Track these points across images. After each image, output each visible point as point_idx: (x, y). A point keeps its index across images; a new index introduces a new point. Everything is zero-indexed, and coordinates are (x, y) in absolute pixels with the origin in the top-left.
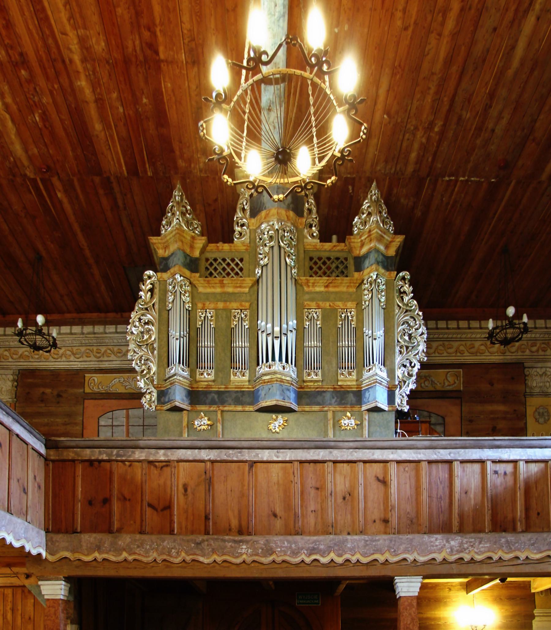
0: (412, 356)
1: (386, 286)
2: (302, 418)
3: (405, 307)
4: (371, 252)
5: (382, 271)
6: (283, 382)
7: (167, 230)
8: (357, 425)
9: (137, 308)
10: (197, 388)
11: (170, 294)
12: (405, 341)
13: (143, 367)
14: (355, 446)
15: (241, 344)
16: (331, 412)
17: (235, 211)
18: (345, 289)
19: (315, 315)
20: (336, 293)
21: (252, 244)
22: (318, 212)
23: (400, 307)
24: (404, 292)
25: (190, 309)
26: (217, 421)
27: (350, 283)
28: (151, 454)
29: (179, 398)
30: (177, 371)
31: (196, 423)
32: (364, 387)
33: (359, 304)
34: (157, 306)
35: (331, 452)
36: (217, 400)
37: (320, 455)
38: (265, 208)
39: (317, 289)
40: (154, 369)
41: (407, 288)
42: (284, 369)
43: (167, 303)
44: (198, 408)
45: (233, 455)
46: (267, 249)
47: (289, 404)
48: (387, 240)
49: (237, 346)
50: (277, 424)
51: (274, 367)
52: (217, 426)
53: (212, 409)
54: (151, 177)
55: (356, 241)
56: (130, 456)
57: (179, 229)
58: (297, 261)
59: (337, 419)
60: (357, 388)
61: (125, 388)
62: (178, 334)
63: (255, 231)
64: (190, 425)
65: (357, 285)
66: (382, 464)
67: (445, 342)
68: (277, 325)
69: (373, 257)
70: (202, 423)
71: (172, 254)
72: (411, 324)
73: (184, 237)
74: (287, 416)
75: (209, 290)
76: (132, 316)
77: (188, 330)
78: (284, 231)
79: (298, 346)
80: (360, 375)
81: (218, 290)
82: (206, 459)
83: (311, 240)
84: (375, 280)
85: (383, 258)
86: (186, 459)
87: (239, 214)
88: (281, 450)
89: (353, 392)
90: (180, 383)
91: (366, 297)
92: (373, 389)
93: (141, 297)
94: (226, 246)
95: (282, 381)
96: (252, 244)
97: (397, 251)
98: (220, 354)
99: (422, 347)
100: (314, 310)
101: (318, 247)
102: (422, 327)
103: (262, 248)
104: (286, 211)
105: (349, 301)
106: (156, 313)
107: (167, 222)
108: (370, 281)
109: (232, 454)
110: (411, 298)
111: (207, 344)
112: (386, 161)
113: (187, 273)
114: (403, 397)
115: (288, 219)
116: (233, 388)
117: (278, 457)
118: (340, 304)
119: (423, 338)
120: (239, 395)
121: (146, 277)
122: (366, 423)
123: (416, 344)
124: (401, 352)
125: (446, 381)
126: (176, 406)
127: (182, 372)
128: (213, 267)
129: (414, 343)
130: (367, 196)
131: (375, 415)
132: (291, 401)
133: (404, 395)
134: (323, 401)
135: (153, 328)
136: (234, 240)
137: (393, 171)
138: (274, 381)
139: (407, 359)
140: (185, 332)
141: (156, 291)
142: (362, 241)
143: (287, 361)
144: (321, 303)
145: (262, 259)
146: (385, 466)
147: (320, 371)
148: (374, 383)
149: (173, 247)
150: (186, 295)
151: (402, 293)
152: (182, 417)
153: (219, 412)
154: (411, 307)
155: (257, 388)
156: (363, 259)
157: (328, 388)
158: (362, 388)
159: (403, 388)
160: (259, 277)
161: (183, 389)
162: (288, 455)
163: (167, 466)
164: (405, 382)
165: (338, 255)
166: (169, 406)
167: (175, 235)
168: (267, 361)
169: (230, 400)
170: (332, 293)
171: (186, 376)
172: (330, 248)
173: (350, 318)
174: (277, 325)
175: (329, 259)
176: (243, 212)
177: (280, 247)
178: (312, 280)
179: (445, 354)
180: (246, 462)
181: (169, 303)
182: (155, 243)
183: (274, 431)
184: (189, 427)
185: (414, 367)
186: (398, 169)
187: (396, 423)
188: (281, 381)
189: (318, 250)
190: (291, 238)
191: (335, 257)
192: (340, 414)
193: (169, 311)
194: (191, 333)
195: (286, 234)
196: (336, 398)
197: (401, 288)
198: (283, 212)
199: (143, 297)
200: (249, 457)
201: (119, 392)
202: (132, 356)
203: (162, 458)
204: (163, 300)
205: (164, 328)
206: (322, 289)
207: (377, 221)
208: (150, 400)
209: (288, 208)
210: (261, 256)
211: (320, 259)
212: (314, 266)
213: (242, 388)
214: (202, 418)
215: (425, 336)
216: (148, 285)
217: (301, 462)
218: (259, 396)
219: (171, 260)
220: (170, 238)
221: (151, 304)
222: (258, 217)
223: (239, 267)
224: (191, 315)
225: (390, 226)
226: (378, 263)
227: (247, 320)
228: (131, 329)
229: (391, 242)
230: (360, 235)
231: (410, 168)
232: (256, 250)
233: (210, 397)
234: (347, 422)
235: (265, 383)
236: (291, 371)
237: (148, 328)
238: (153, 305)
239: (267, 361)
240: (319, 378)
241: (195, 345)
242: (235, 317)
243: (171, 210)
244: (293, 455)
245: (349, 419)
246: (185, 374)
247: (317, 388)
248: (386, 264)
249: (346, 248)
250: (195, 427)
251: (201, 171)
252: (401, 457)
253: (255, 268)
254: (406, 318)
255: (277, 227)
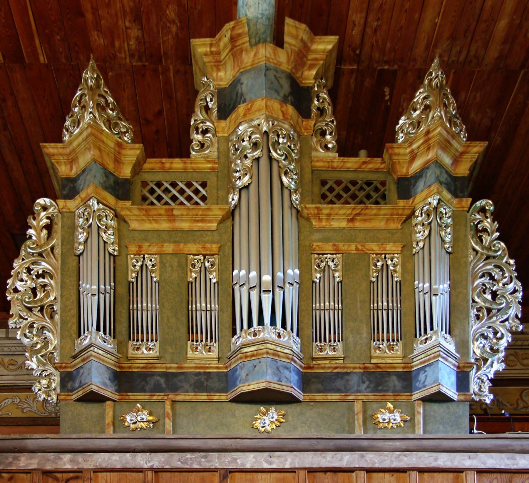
0: (498, 322)
1: (453, 220)
2: (310, 413)
3: (485, 252)
4: (428, 168)
5: (447, 195)
6: (279, 356)
7: (74, 133)
8: (405, 421)
9: (23, 253)
10: (130, 368)
11: (81, 231)
12: (485, 300)
13: (35, 339)
14: (404, 447)
15: (205, 307)
16: (360, 402)
17: (191, 112)
18: (382, 224)
19: (331, 264)
20: (368, 230)
21: (222, 160)
22: (334, 113)
23: (477, 252)
24: (485, 230)
25: (116, 253)
26: (165, 415)
27: (392, 214)
28: (49, 460)
29: (97, 380)
30: (93, 340)
31: (128, 418)
32: (416, 366)
33: (406, 246)
34: (58, 251)
35: (363, 456)
36: (164, 386)
37: (345, 460)
38: (244, 101)
39: (335, 224)
40: (54, 341)
41: (487, 223)
42: (279, 336)
43: (76, 245)
44: (132, 397)
45: (194, 461)
46: (248, 162)
47: (290, 389)
48: (457, 150)
49: (198, 308)
50: (267, 419)
51: (262, 334)
52: (164, 424)
53: (155, 398)
54: (46, 66)
55: (402, 151)
56: (11, 464)
57: (93, 125)
58: (300, 183)
59: (369, 412)
60: (404, 368)
61: (23, 412)
62: (95, 287)
63: (228, 139)
64: (118, 423)
65: (404, 217)
66: (451, 475)
67: (518, 351)
68: (266, 277)
69: (431, 174)
70: (139, 419)
71: (83, 171)
72: (496, 277)
73: (103, 142)
74: (284, 409)
75: (147, 226)
76: (15, 265)
77: (112, 284)
78: (278, 136)
79: (303, 308)
80: (408, 349)
81: (165, 225)
82: (145, 466)
83: (325, 154)
84: (436, 208)
85: (449, 179)
86: (109, 467)
87: (199, 115)
88: (276, 454)
89: (397, 374)
90: (100, 359)
91: (418, 235)
92: (432, 367)
93: (30, 237)
94: (177, 164)
95: (276, 354)
96: (222, 160)
97: (472, 169)
98: (168, 320)
99: (515, 310)
100: (329, 256)
101: (335, 165)
102: (515, 280)
103: (239, 161)
104: (281, 104)
105: (389, 242)
106: (57, 260)
107: (73, 122)
108: (427, 210)
109: (191, 459)
110: (496, 239)
111: (146, 307)
112: (453, 38)
113: (111, 200)
114: (482, 381)
115: (285, 118)
116: (191, 368)
117: (270, 463)
118: (375, 247)
119: (517, 298)
120: (203, 378)
121: (37, 208)
122: (420, 418)
123: (503, 305)
124: (478, 317)
125: (520, 402)
126: (92, 392)
127: (103, 343)
128: (155, 195)
129: (502, 304)
130: (422, 82)
131: (435, 407)
132: (292, 385)
133: (485, 379)
134: (345, 388)
135: (52, 282)
136: (190, 153)
137: (462, 58)
138: (263, 354)
139: (489, 327)
140: (108, 287)
141: (58, 228)
142: (413, 151)
143: (284, 326)
144: (341, 245)
145: (240, 178)
146: (457, 478)
147: (340, 344)
148: (435, 357)
149: (84, 159)
150: (109, 232)
151: (479, 233)
152: (105, 410)
153: (168, 403)
154: (496, 251)
155: (232, 367)
156: (413, 181)
157: (354, 368)
158: (412, 367)
159: (483, 369)
160: (236, 206)
161: (104, 369)
162: (289, 460)
163: (77, 478)
164: (485, 360)
165: (370, 177)
166: (81, 393)
167: (87, 137)
168: (250, 325)
169: (187, 386)
170: (360, 230)
171: (111, 350)
172: (356, 166)
173: (391, 268)
174: (266, 277)
175: (354, 183)
176: (207, 113)
177: (271, 159)
178: (326, 209)
179: (519, 366)
180: (215, 470)
181: (80, 244)
182: (53, 155)
183: (263, 429)
184: (116, 424)
185: (501, 338)
186: (472, 53)
187: (471, 420)
188: (274, 354)
189: (334, 170)
190: (289, 146)
191: (364, 181)
192: (375, 406)
193: (79, 256)
194: (118, 289)
195: (281, 140)
196: (367, 383)
197: (478, 223)
198: (276, 106)
199: (34, 238)
200: (220, 463)
201: (13, 416)
202: (15, 323)
203: (68, 466)
204: (69, 240)
205: (71, 281)
206: (344, 224)
207: (441, 117)
208: (48, 387)
209: (284, 100)
210: (238, 174)
211: (338, 183)
212: (328, 194)
213: (207, 368)
214: (139, 411)
215: (520, 295)
216: (41, 220)
217: (311, 471)
218: (236, 379)
219: (81, 182)
220: (79, 145)
221: (48, 247)
222: (233, 116)
223: (200, 195)
224: (118, 262)
225: (461, 131)
226: (441, 183)
227: (215, 271)
228: (13, 284)
229: (462, 153)
230: (409, 142)
231: (493, 52)
232: (229, 167)
233: (152, 381)
234: (387, 416)
235: (246, 357)
236: (291, 342)
237: (42, 282)
238: (52, 249)
239: (250, 325)
240: (339, 353)
241: (126, 306)
242: (193, 266)
243: (80, 102)
244: (297, 460)
245: (391, 412)
246: (110, 347)
247: (336, 368)
248: (453, 189)
249: (383, 166)
250: (126, 424)
251: (132, 56)
252: (485, 464)
253: (228, 193)
254: (489, 267)
255: (265, 129)
